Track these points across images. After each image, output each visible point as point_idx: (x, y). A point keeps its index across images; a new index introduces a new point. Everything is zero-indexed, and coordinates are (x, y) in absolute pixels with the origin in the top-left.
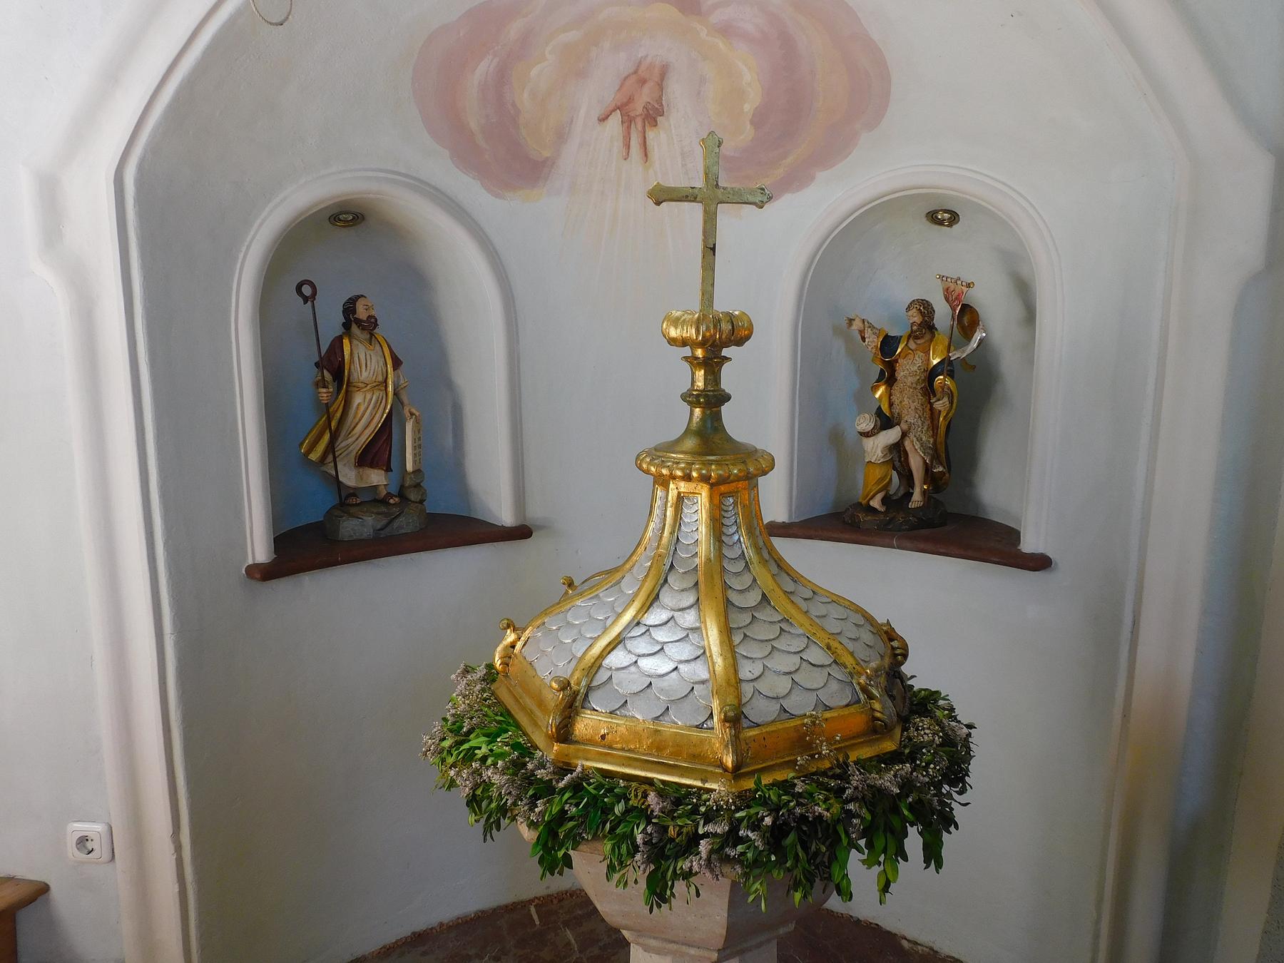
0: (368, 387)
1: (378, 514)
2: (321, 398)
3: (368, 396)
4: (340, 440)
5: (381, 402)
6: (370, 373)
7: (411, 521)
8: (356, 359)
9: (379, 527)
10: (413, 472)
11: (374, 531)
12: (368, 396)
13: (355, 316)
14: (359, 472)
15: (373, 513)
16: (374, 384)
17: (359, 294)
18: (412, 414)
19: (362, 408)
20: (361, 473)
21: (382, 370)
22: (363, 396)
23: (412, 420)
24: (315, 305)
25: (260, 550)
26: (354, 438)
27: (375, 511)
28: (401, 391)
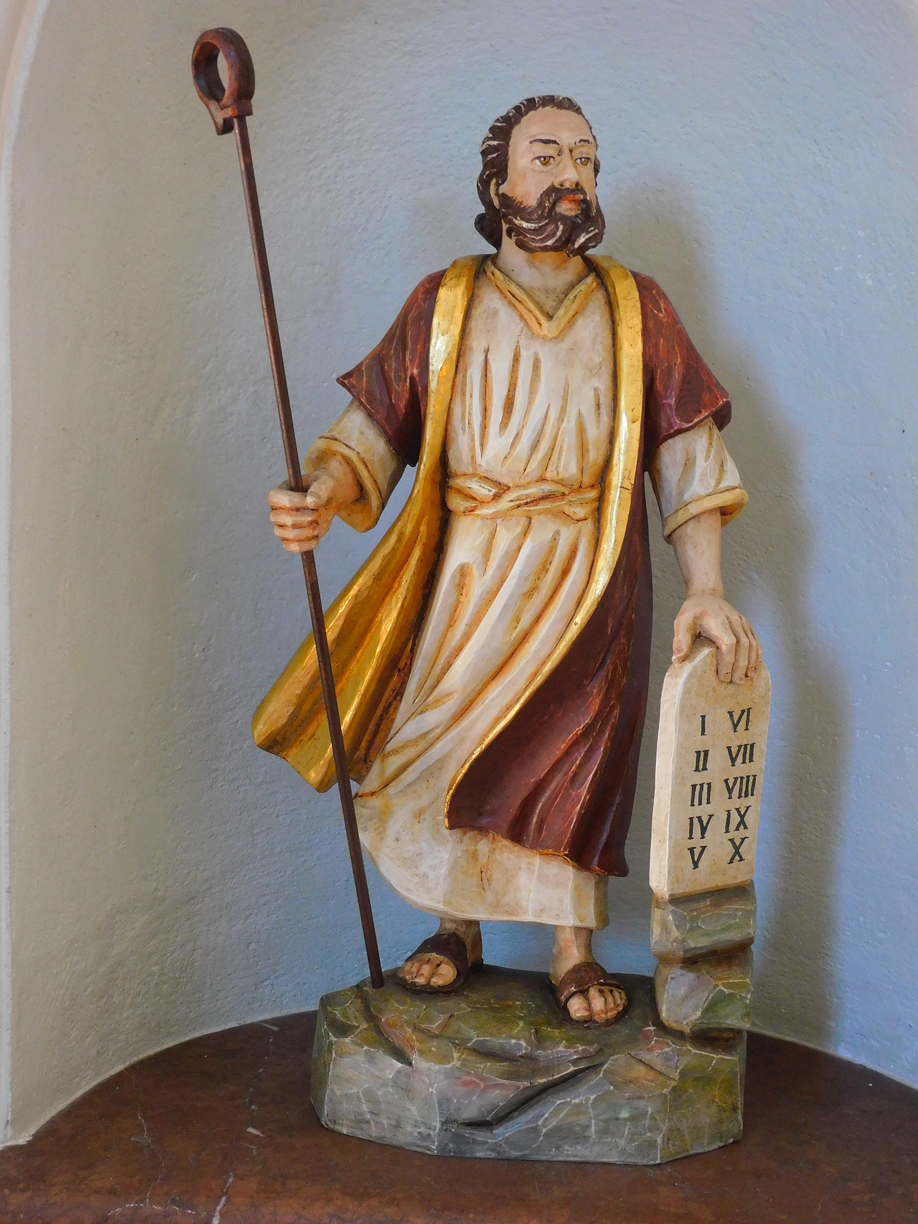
0: (504, 503)
1: (486, 1053)
2: (278, 532)
3: (504, 539)
4: (405, 707)
5: (565, 572)
6: (517, 436)
7: (624, 1114)
8: (474, 374)
9: (471, 1112)
10: (676, 900)
11: (446, 1122)
12: (504, 539)
13: (503, 189)
14: (475, 856)
15: (460, 1044)
16: (535, 491)
17: (578, 100)
18: (700, 638)
19: (477, 588)
20: (483, 860)
21: (581, 431)
22: (486, 533)
23: (688, 667)
24: (210, 116)
25: (693, 867)
26: (450, 707)
27: (475, 1037)
28: (690, 529)
